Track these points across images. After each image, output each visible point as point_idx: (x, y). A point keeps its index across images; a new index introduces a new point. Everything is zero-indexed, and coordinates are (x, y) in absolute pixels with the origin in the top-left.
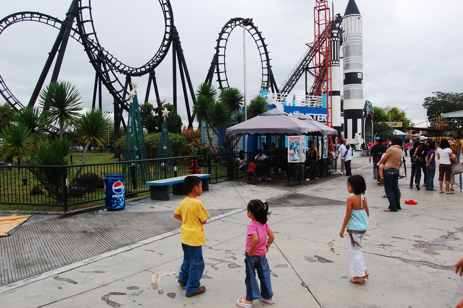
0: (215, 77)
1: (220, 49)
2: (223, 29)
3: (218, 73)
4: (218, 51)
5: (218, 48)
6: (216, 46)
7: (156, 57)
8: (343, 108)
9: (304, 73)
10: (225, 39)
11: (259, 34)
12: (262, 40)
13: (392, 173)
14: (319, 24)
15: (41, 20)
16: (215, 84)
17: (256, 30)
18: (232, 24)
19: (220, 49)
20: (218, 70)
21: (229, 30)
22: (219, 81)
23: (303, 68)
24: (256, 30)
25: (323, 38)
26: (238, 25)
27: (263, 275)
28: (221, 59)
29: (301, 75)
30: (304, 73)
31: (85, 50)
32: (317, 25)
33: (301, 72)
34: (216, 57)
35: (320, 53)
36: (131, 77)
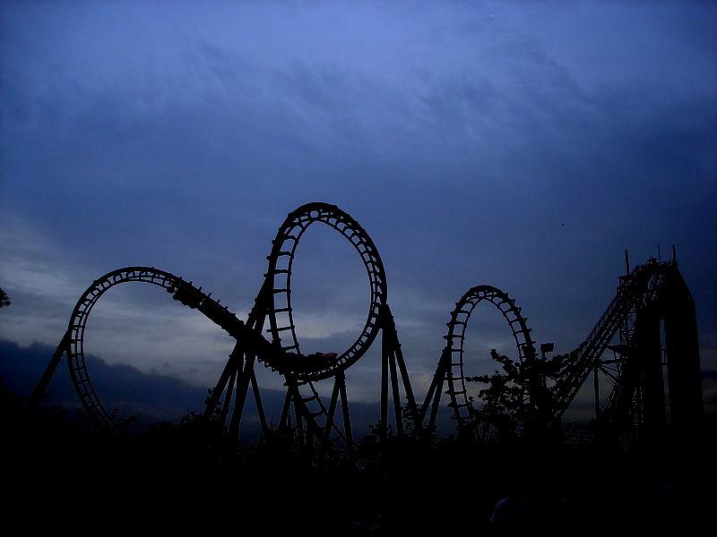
0: (445, 387)
2: (282, 229)
3: (450, 380)
4: (450, 343)
5: (449, 337)
9: (593, 372)
11: (517, 311)
12: (522, 321)
13: (332, 368)
16: (445, 400)
17: (512, 305)
18: (302, 218)
20: (450, 374)
21: (296, 231)
22: (451, 392)
24: (512, 305)
25: (613, 322)
28: (455, 357)
30: (593, 372)
34: (447, 353)
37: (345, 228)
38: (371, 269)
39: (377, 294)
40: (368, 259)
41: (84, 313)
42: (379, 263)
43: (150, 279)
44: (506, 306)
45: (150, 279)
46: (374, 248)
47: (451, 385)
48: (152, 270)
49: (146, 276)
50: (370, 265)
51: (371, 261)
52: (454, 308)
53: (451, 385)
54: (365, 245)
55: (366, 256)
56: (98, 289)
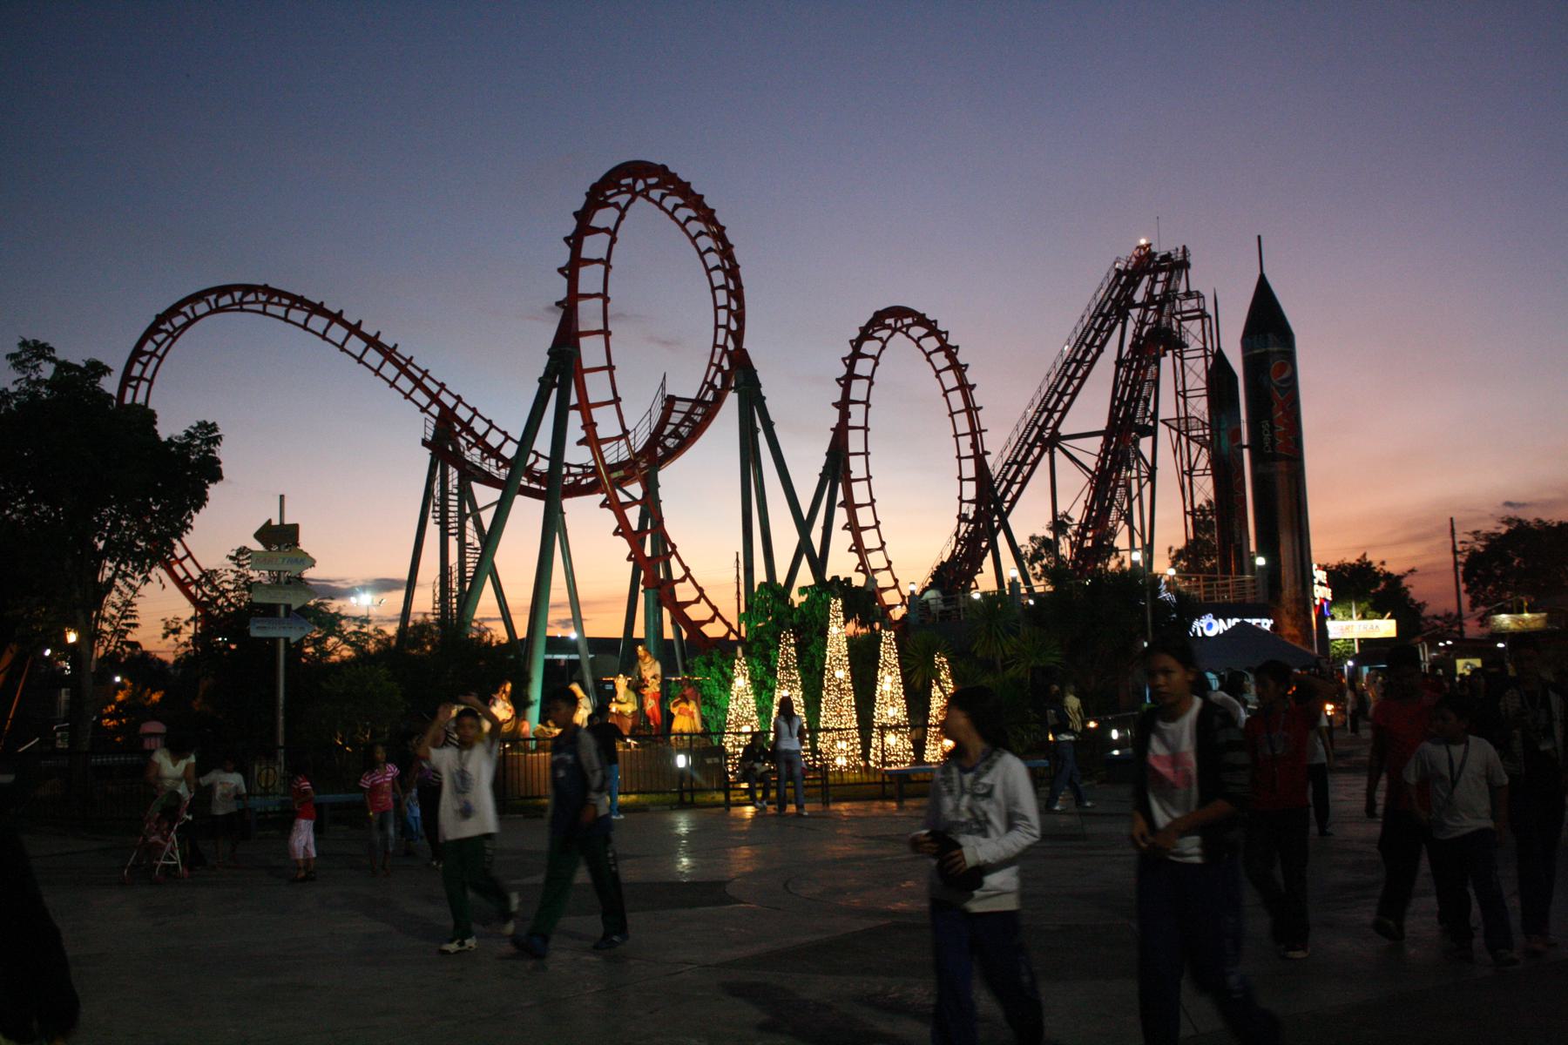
1: (852, 408)
3: (585, 407)
4: (845, 415)
6: (838, 398)
7: (160, 353)
8: (1370, 779)
9: (1046, 456)
10: (599, 261)
14: (1185, 397)
15: (270, 309)
19: (852, 408)
23: (1039, 437)
26: (640, 193)
27: (1412, 601)
29: (1035, 464)
30: (1046, 456)
31: (425, 443)
32: (1181, 400)
33: (1036, 451)
35: (1189, 438)
36: (828, 578)
37: (717, 268)
38: (720, 341)
39: (712, 386)
40: (723, 320)
41: (153, 354)
42: (740, 316)
43: (260, 307)
44: (931, 343)
45: (260, 307)
46: (739, 286)
47: (589, 425)
48: (266, 289)
49: (256, 301)
50: (722, 332)
51: (727, 327)
52: (570, 226)
53: (589, 425)
54: (730, 294)
55: (723, 314)
56: (185, 314)
